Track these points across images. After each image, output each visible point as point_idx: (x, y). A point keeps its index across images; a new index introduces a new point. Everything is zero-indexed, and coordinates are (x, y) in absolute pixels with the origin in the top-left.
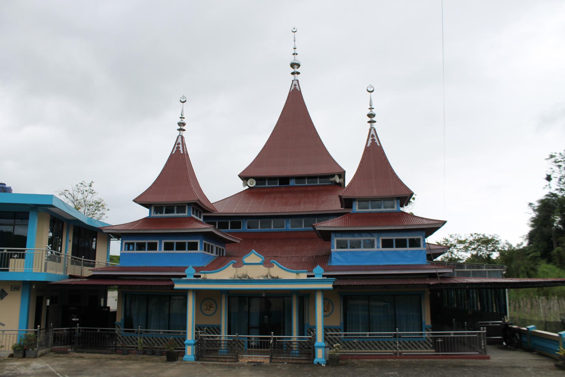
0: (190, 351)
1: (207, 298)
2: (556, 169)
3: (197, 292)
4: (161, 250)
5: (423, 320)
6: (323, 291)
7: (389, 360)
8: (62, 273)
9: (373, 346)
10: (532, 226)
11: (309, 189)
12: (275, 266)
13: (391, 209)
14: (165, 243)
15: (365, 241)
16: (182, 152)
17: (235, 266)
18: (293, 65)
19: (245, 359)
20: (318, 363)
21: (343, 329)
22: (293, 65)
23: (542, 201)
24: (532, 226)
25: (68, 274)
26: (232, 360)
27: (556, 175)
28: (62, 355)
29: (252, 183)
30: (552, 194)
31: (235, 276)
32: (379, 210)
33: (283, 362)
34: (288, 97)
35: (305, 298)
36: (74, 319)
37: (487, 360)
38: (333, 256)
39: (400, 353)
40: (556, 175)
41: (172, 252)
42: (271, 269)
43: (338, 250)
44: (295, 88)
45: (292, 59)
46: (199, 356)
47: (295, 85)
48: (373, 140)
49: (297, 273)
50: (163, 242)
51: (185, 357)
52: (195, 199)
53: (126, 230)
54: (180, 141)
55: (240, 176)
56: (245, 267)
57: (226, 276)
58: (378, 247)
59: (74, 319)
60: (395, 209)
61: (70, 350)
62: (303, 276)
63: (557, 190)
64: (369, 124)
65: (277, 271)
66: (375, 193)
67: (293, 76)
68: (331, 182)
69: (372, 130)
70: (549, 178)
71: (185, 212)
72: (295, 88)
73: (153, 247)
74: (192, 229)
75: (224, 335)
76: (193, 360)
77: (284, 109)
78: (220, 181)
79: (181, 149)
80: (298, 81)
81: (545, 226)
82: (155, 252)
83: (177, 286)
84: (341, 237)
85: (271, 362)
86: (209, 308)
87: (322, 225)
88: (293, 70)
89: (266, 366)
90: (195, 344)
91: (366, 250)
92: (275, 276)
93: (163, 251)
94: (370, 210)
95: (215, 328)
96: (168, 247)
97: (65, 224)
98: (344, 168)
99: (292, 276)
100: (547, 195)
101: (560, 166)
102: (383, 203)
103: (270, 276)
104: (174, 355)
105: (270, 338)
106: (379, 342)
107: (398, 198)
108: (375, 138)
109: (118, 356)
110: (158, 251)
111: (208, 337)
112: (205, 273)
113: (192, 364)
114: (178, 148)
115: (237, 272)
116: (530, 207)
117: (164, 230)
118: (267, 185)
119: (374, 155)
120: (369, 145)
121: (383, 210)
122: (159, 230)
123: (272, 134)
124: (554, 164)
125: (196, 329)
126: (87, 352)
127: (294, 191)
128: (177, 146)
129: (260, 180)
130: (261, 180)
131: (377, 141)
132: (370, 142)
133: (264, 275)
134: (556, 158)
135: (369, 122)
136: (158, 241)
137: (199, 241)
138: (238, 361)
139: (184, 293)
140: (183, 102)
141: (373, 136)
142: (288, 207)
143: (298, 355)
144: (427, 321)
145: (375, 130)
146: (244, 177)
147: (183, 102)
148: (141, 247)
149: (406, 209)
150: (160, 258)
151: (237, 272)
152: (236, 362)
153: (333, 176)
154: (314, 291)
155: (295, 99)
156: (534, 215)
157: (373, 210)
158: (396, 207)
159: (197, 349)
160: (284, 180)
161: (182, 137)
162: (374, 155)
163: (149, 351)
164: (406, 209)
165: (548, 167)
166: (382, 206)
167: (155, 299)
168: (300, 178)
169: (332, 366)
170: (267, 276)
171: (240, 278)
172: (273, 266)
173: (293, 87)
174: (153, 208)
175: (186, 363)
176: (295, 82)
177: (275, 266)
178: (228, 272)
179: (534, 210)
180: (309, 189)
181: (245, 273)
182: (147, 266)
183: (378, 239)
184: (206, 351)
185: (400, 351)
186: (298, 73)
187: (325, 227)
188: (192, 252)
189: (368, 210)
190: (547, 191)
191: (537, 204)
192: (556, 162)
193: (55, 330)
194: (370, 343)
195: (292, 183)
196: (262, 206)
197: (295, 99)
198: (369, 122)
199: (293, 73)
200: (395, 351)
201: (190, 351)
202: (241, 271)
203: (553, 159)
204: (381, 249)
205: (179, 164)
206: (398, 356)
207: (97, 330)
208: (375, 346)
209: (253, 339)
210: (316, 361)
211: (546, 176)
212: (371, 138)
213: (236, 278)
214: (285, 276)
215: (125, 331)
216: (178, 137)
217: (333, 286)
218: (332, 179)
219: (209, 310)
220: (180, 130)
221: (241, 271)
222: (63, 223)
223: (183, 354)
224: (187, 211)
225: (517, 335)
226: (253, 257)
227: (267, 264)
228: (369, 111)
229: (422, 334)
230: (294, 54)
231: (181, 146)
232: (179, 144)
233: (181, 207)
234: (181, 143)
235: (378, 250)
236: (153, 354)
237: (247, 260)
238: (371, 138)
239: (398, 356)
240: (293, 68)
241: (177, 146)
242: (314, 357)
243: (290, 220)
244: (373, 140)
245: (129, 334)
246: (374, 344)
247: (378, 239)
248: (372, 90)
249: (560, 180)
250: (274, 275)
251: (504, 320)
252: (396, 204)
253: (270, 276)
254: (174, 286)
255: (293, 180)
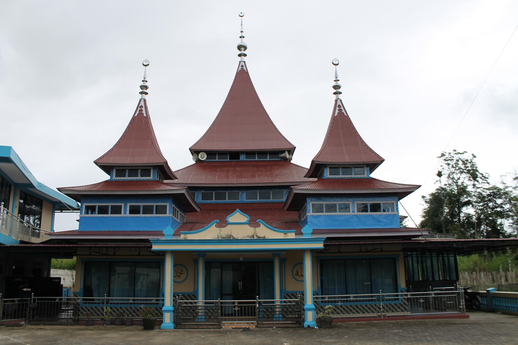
0: (168, 319)
1: (186, 261)
2: (446, 167)
3: (175, 253)
4: (125, 214)
5: (399, 283)
6: (313, 251)
7: (376, 322)
8: (15, 238)
9: (351, 310)
10: (424, 217)
11: (260, 164)
12: (261, 225)
13: (362, 176)
14: (130, 206)
15: (340, 205)
16: (145, 115)
17: (219, 226)
18: (240, 47)
19: (227, 325)
20: (309, 326)
21: (321, 294)
22: (240, 47)
23: (433, 195)
24: (424, 217)
25: (19, 240)
26: (214, 327)
27: (446, 173)
28: (16, 328)
29: (203, 157)
30: (442, 188)
31: (218, 237)
32: (350, 176)
33: (272, 327)
34: (236, 77)
35: (292, 259)
36: (25, 290)
37: (467, 319)
38: (309, 220)
39: (384, 316)
40: (446, 173)
41: (138, 215)
42: (257, 228)
43: (314, 214)
44: (242, 69)
45: (239, 42)
46: (178, 323)
47: (242, 66)
48: (340, 110)
49: (285, 233)
50: (128, 205)
51: (163, 325)
52: (162, 161)
53: (90, 191)
54: (142, 103)
55: (191, 150)
56: (229, 226)
57: (208, 236)
58: (353, 212)
59: (25, 290)
60: (365, 176)
61: (23, 323)
62: (292, 235)
63: (445, 185)
64: (335, 96)
65: (264, 231)
66: (347, 159)
67: (240, 58)
68: (281, 157)
69: (339, 101)
70: (440, 174)
71: (150, 176)
72: (242, 69)
73: (117, 210)
74: (159, 190)
75: (201, 301)
76: (173, 328)
77: (232, 88)
78: (176, 150)
79: (144, 112)
80: (245, 62)
81: (437, 216)
82: (119, 215)
83: (155, 247)
84: (316, 201)
85: (257, 327)
86: (178, 275)
87: (299, 188)
88: (240, 52)
89: (253, 331)
90: (174, 311)
91: (341, 214)
92: (262, 236)
93: (128, 214)
94: (341, 176)
95: (186, 295)
96: (134, 210)
97: (13, 188)
98: (295, 144)
99: (280, 236)
100: (437, 189)
101: (449, 164)
102: (354, 170)
103: (257, 236)
104: (151, 324)
105: (254, 303)
106: (357, 306)
107: (367, 165)
108: (342, 108)
109: (83, 327)
110: (122, 215)
111: (186, 303)
112: (185, 234)
113: (171, 331)
114: (141, 111)
115: (220, 232)
116: (423, 199)
117: (133, 191)
118: (217, 160)
119: (341, 126)
120: (336, 115)
121: (353, 176)
122: (127, 191)
123: (221, 111)
124: (444, 161)
125: (174, 296)
126: (44, 325)
127: (243, 164)
128: (139, 109)
129: (210, 154)
130: (208, 155)
131: (343, 111)
132: (337, 112)
133: (250, 235)
134: (446, 157)
135: (335, 93)
136: (123, 205)
137: (168, 204)
138: (221, 328)
139: (162, 254)
140: (146, 66)
141: (339, 106)
142: (243, 179)
143: (281, 319)
144: (402, 284)
145: (341, 101)
146: (194, 151)
147: (146, 66)
148: (103, 210)
149: (375, 175)
150: (124, 223)
151: (220, 232)
152: (220, 328)
153: (283, 152)
154: (303, 251)
155: (242, 78)
156: (426, 206)
157: (344, 176)
158: (366, 174)
159: (174, 316)
160: (235, 155)
161: (145, 101)
162: (341, 126)
163: (120, 322)
164: (375, 175)
165: (439, 164)
166: (353, 173)
167: (138, 259)
168: (250, 153)
169: (325, 328)
170: (253, 236)
171: (224, 238)
172: (259, 226)
173: (240, 68)
174: (114, 171)
175: (166, 331)
176: (242, 63)
177: (261, 225)
178: (211, 232)
179: (426, 202)
180: (260, 164)
181: (229, 234)
182: (111, 230)
183: (353, 203)
184: (184, 318)
185: (384, 314)
186: (245, 55)
187: (303, 189)
188: (160, 215)
189: (339, 176)
190: (437, 186)
191: (428, 197)
192: (445, 160)
193: (5, 301)
194: (348, 308)
195: (242, 158)
196: (217, 178)
197: (242, 78)
198: (335, 93)
199: (240, 55)
200: (380, 314)
201: (168, 319)
202: (225, 232)
203: (444, 158)
204: (356, 213)
205: (140, 127)
206: (382, 317)
207: (55, 299)
208: (353, 310)
209: (236, 304)
210: (306, 324)
211: (437, 172)
212: (337, 108)
213: (220, 239)
214: (271, 236)
215: (84, 300)
216: (140, 100)
217: (324, 245)
218: (283, 155)
219: (179, 277)
220: (141, 93)
221: (225, 232)
222: (10, 187)
223: (161, 322)
224: (152, 174)
225: (478, 297)
226: (238, 217)
227: (253, 223)
228: (334, 83)
229: (397, 296)
230: (240, 37)
231: (143, 109)
232: (142, 107)
233: (145, 170)
234: (143, 106)
235: (353, 214)
236: (123, 323)
237: (231, 219)
238: (337, 108)
239: (382, 317)
240: (240, 50)
241: (139, 109)
242: (304, 321)
243: (245, 191)
244: (340, 110)
245: (89, 306)
246: (351, 308)
247: (353, 203)
248: (337, 63)
249: (449, 175)
250: (261, 235)
251: (456, 286)
252: (366, 169)
253: (257, 236)
254: (151, 247)
255: (243, 155)
